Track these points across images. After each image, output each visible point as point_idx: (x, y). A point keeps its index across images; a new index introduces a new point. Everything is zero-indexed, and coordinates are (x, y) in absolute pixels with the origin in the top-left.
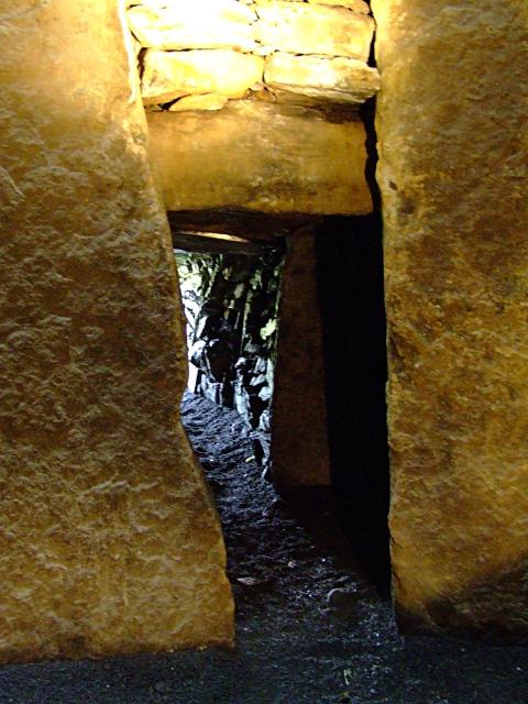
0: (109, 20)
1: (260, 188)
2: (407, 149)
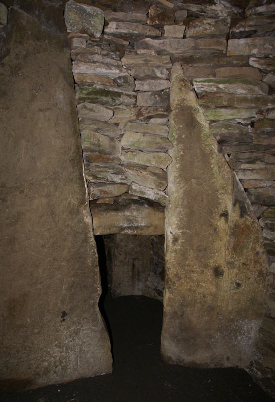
0: (80, 177)
1: (125, 227)
2: (177, 222)
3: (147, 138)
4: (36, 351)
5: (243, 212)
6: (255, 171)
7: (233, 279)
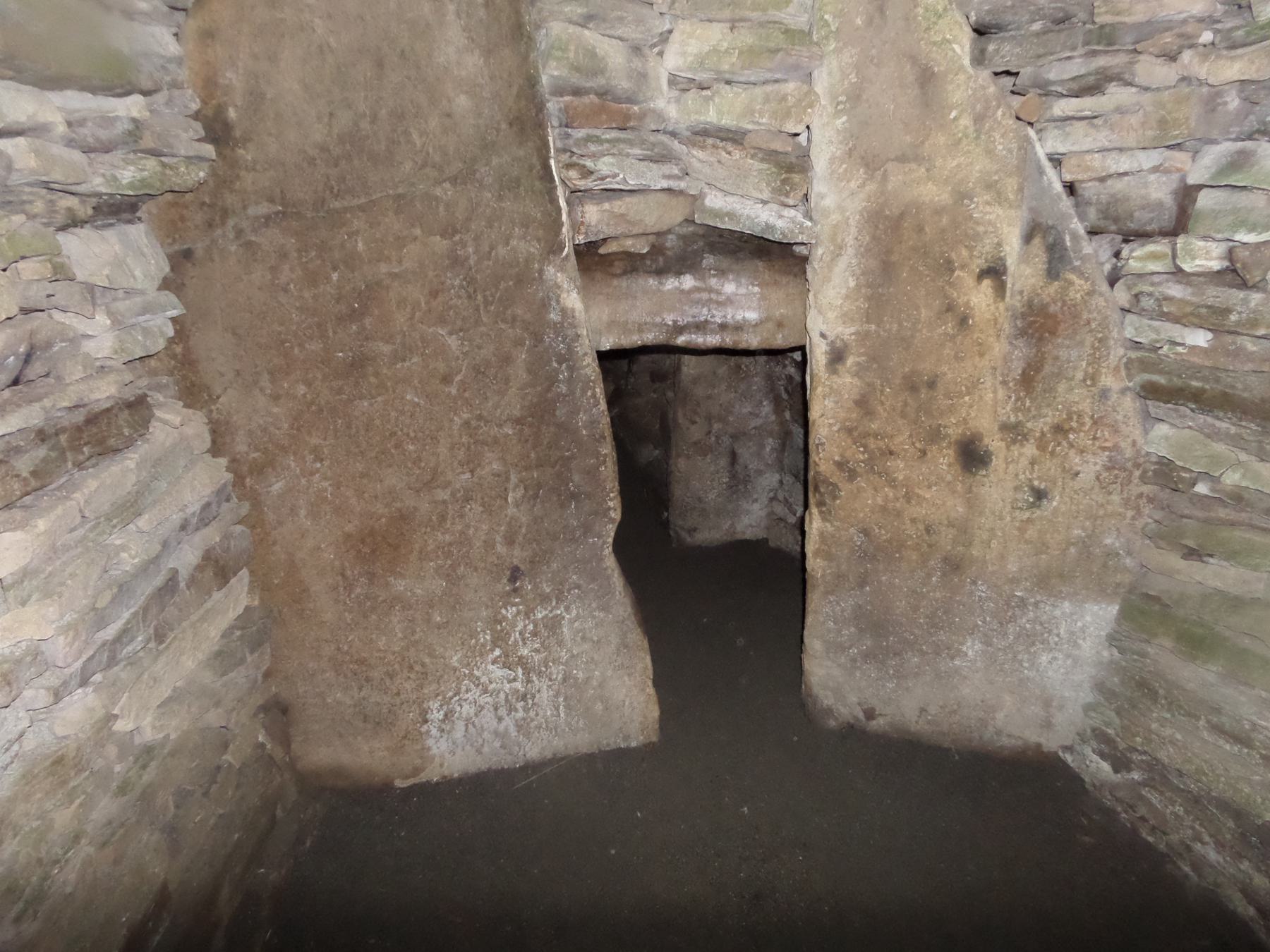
3: (746, 38)
4: (442, 676)
5: (1057, 259)
6: (1098, 122)
7: (1022, 477)
